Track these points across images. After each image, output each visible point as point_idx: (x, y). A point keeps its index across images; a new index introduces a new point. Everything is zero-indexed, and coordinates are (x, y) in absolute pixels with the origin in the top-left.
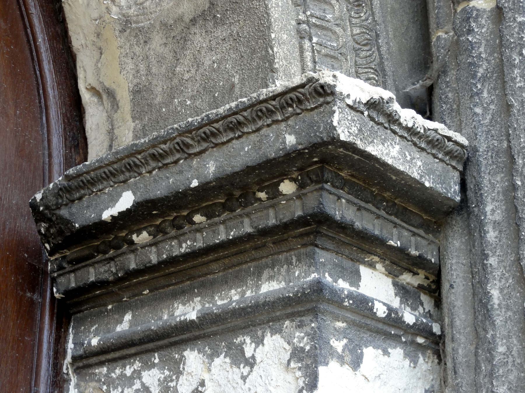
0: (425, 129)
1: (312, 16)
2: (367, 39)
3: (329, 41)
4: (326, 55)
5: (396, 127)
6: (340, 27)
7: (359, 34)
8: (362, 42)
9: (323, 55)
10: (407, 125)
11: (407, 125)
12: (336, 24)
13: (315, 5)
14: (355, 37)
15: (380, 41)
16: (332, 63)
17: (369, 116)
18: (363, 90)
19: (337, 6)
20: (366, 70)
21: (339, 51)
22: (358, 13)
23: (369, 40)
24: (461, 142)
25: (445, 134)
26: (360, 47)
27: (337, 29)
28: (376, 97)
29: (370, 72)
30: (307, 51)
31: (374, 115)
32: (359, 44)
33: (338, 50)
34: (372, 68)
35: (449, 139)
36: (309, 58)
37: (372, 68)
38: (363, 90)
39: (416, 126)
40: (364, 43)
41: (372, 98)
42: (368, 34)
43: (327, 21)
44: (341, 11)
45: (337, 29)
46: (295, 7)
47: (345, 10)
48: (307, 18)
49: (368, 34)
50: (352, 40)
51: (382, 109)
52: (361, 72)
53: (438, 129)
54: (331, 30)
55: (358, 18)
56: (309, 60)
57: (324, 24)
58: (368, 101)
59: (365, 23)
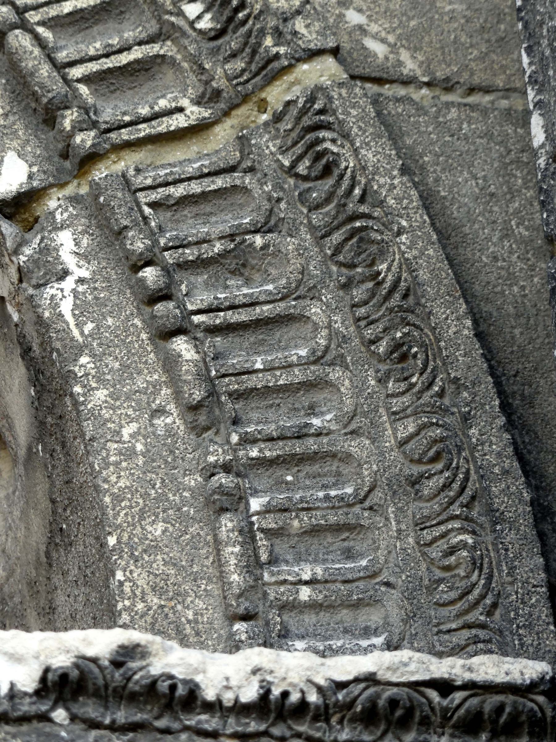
0: (320, 689)
1: (247, 440)
2: (435, 441)
3: (335, 485)
4: (314, 531)
5: (203, 717)
6: (363, 434)
7: (417, 433)
8: (425, 453)
9: (298, 535)
10: (237, 700)
11: (237, 700)
12: (352, 432)
13: (271, 406)
14: (408, 447)
15: (473, 431)
16: (346, 544)
17: (73, 718)
18: (16, 658)
19: (347, 382)
20: (443, 528)
21: (367, 504)
22: (406, 379)
23: (442, 440)
24: (501, 679)
25: (414, 678)
26: (423, 468)
27: (353, 446)
28: (62, 661)
29: (452, 530)
30: (227, 544)
31: (90, 709)
32: (419, 461)
33: (362, 502)
34: (457, 517)
35: (445, 686)
36: (233, 561)
37: (457, 517)
38: (16, 658)
39: (276, 692)
40: (431, 453)
41: (47, 670)
42: (437, 424)
43: (319, 435)
44: (358, 390)
45: (353, 446)
46: (199, 435)
47: (373, 383)
48: (235, 451)
49: (437, 424)
50: (401, 459)
51: (106, 686)
52: (429, 538)
53: (374, 674)
54: (334, 456)
55: (407, 390)
56: (232, 568)
57: (312, 444)
58: (43, 680)
59: (426, 397)
